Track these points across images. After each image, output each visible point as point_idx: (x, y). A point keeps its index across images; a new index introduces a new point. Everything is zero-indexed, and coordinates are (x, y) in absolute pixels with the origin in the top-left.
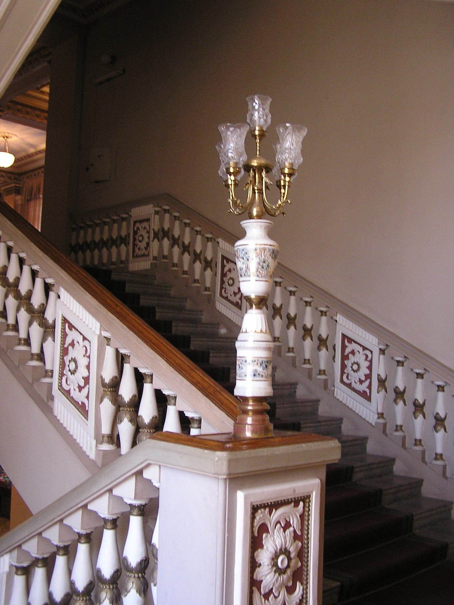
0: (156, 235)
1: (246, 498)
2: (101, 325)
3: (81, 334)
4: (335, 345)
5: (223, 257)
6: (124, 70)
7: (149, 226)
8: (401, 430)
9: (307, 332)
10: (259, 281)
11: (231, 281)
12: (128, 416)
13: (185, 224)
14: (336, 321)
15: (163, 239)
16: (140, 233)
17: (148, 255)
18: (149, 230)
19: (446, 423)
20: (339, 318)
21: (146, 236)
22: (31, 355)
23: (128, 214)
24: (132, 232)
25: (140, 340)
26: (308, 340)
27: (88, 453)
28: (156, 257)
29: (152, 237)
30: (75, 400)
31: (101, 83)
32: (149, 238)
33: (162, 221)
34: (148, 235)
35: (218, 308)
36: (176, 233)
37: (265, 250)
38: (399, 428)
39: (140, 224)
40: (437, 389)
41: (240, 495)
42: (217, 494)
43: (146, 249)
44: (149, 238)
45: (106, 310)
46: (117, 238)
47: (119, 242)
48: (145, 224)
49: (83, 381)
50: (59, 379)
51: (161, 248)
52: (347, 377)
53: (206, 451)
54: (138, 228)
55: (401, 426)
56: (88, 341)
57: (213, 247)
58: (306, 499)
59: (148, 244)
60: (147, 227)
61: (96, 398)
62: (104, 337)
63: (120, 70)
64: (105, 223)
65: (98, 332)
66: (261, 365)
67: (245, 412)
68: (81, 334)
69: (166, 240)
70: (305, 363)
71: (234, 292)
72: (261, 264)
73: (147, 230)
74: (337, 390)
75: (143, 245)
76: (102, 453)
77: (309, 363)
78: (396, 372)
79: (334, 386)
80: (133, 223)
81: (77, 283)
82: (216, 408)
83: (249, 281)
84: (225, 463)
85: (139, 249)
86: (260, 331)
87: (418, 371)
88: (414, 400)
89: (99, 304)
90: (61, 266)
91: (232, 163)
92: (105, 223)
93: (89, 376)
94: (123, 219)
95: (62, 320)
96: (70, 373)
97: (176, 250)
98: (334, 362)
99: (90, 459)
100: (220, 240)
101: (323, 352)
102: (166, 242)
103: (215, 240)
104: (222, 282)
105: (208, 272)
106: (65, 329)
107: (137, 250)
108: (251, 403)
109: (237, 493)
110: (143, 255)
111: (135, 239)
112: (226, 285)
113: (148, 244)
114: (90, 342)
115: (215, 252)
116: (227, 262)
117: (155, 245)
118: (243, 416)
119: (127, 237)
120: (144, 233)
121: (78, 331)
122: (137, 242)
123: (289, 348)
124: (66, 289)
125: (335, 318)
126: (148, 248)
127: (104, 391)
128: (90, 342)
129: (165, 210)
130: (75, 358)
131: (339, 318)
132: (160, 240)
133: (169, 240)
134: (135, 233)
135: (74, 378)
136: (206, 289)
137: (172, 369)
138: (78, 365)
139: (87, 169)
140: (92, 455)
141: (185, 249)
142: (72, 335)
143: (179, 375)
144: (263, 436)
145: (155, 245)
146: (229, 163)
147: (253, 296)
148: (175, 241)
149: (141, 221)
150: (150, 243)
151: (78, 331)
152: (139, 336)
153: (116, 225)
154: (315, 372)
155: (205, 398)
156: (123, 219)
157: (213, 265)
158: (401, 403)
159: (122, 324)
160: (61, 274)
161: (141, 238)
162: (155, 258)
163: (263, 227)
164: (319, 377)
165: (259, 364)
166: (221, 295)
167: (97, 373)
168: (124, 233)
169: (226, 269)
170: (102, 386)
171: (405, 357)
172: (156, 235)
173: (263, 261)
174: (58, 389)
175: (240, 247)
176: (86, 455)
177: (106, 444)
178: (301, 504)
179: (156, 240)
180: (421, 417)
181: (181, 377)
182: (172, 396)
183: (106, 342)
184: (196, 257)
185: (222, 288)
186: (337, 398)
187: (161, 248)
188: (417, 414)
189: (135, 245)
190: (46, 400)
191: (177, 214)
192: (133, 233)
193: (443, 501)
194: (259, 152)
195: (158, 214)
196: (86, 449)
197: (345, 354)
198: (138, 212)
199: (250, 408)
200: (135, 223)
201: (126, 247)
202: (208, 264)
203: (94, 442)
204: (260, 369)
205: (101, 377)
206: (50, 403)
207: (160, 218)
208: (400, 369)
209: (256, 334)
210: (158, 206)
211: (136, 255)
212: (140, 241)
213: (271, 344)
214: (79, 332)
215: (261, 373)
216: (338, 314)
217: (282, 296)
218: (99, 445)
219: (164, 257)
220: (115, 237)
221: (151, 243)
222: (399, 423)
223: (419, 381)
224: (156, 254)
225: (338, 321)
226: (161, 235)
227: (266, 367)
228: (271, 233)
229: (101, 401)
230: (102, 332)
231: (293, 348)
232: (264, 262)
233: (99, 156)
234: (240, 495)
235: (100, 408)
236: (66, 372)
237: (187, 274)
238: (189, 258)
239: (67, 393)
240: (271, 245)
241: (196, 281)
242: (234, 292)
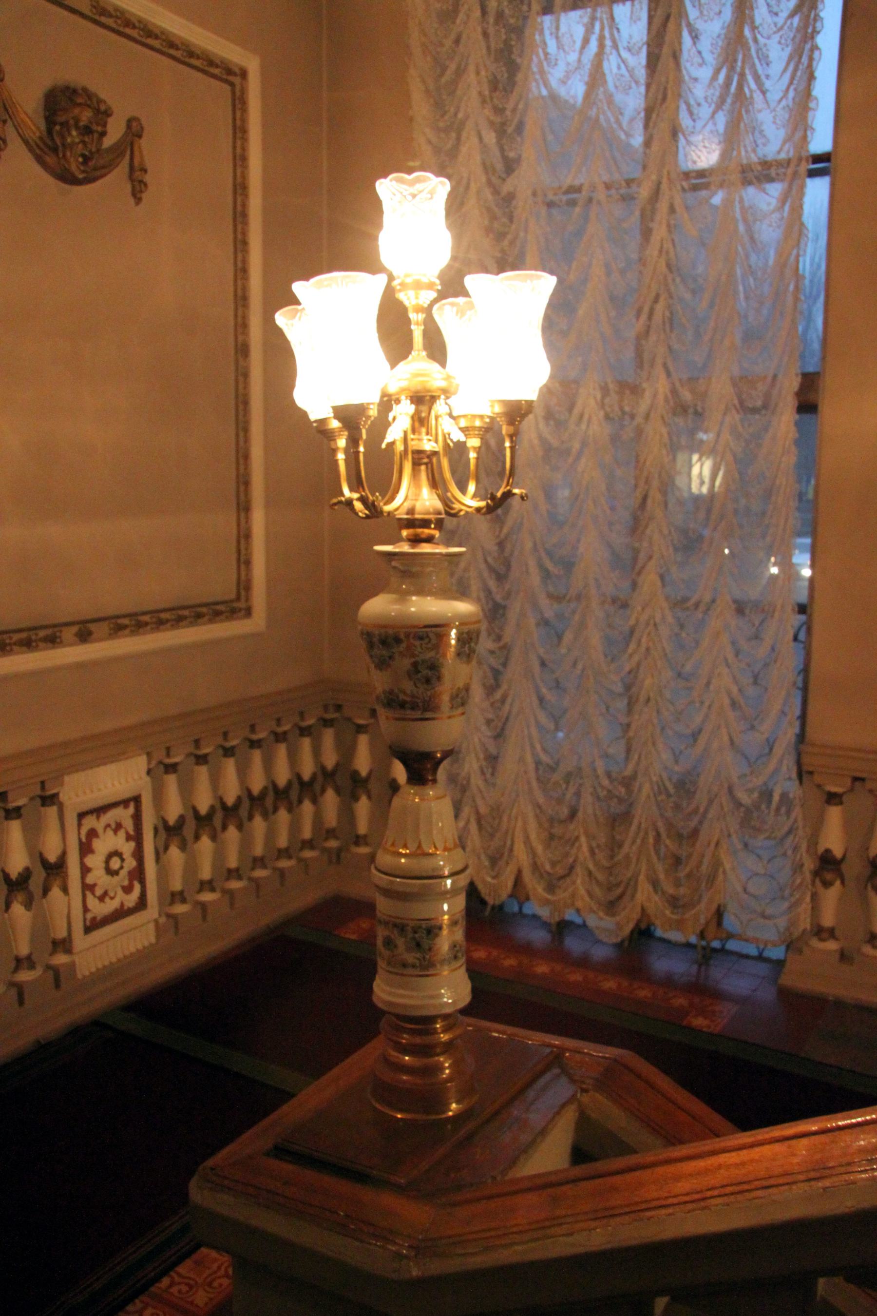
21: (98, 876)
32: (85, 870)
60: (92, 902)
73: (93, 894)
75: (104, 844)
107: (129, 825)
113: (86, 849)
122: (128, 848)
126: (84, 840)
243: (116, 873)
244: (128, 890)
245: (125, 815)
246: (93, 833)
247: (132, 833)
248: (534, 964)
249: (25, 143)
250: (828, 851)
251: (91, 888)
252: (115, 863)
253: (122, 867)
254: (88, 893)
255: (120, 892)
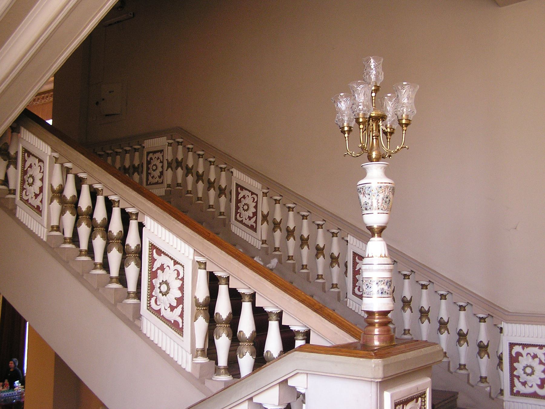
0: (170, 165)
1: (392, 396)
2: (194, 250)
3: (172, 259)
4: (347, 262)
5: (238, 186)
6: (133, 14)
7: (163, 156)
8: (409, 333)
9: (319, 251)
10: (383, 213)
11: (246, 207)
12: (225, 332)
13: (199, 155)
14: (347, 241)
15: (177, 169)
16: (153, 163)
17: (162, 183)
18: (163, 160)
19: (448, 325)
20: (350, 238)
22: (127, 293)
23: (140, 145)
24: (146, 162)
25: (241, 264)
26: (321, 258)
27: (184, 366)
28: (170, 185)
29: (166, 167)
30: (167, 318)
31: (110, 25)
32: (162, 167)
33: (175, 152)
34: (161, 164)
35: (233, 231)
36: (190, 163)
37: (387, 187)
38: (407, 332)
39: (153, 155)
40: (440, 297)
41: (387, 395)
42: (370, 395)
43: (160, 177)
44: (162, 167)
45: (201, 237)
46: (129, 167)
47: (131, 170)
48: (159, 155)
49: (175, 301)
50: (148, 300)
51: (175, 177)
52: (359, 290)
53: (361, 359)
54: (151, 159)
55: (409, 330)
56: (181, 265)
57: (226, 178)
58: (422, 395)
59: (162, 173)
61: (191, 317)
62: (197, 261)
63: (131, 14)
64: (117, 153)
65: (191, 257)
66: (386, 284)
67: (372, 324)
68: (172, 259)
69: (179, 169)
70: (318, 278)
71: (249, 216)
72: (385, 199)
74: (350, 301)
75: (157, 173)
76: (199, 366)
77: (322, 278)
78: (403, 284)
79: (346, 298)
80: (146, 153)
81: (165, 213)
82: (326, 321)
83: (373, 213)
84: (381, 369)
85: (153, 177)
86: (384, 256)
87: (423, 283)
88: (420, 307)
89: (193, 232)
90: (147, 198)
91: (361, 115)
92: (117, 153)
93: (183, 296)
94: (136, 150)
95: (149, 246)
96: (161, 294)
97: (190, 179)
98: (347, 277)
99: (187, 372)
100: (233, 170)
101: (336, 269)
102: (180, 171)
103: (228, 170)
104: (237, 208)
105: (223, 199)
106: (152, 254)
107: (150, 178)
108: (377, 314)
109: (383, 393)
110: (157, 183)
111: (148, 169)
112: (26, 186)
113: (162, 173)
114: (183, 266)
115: (229, 180)
116: (29, 156)
117: (169, 175)
118: (371, 328)
119: (140, 167)
120: (158, 163)
121: (168, 256)
122: (151, 171)
123: (303, 266)
124: (152, 218)
125: (346, 238)
126: (162, 176)
127: (197, 310)
128: (183, 266)
129: (178, 142)
130: (166, 281)
131: (350, 238)
132: (174, 170)
133: (182, 169)
134: (149, 163)
135: (166, 299)
136: (221, 214)
137: (279, 290)
138: (171, 287)
139: (97, 103)
140: (189, 369)
141: (199, 177)
142: (160, 260)
143: (286, 294)
144: (389, 345)
145: (169, 175)
146: (358, 114)
147: (375, 226)
148: (188, 171)
149: (154, 152)
150: (164, 172)
151: (168, 256)
152: (240, 261)
153: (128, 155)
154: (328, 286)
155: (315, 313)
156: (136, 150)
157: (227, 192)
158: (408, 310)
159: (219, 250)
160: (148, 204)
161: (154, 168)
162: (169, 186)
163: (383, 168)
164: (333, 290)
165: (385, 283)
166: (236, 219)
167: (192, 294)
168: (137, 163)
169: (27, 165)
170: (196, 306)
171: (412, 271)
172: (170, 165)
173: (386, 197)
174: (146, 309)
175: (361, 186)
176: (182, 368)
177: (200, 357)
178: (420, 399)
179: (170, 169)
180: (426, 321)
181: (288, 296)
182: (274, 313)
183: (198, 266)
184: (210, 185)
185: (237, 213)
186: (350, 307)
187: (175, 177)
188: (423, 319)
189: (148, 174)
190: (131, 319)
191: (190, 146)
192: (147, 163)
193: (449, 392)
194: (375, 103)
195: (171, 146)
196: (182, 362)
197: (356, 270)
198: (151, 144)
199: (376, 321)
200: (148, 153)
201: (139, 175)
202: (221, 192)
203: (190, 356)
204: (386, 288)
205: (195, 297)
206: (137, 322)
207: (173, 149)
208: (407, 281)
209: (382, 258)
210: (172, 139)
211: (150, 183)
212: (154, 170)
213: (391, 266)
214: (170, 257)
215: (387, 291)
216: (349, 235)
217: (295, 220)
218: (194, 359)
219: (178, 185)
220: (127, 166)
221: (165, 172)
222: (407, 327)
223: (424, 291)
224: (169, 182)
225: (349, 242)
226: (174, 165)
227: (390, 286)
228: (387, 173)
229: (196, 319)
230: (195, 257)
231: (306, 266)
232: (387, 198)
233: (110, 92)
234: (387, 395)
235: (194, 324)
236: (156, 293)
237: (201, 200)
238: (203, 186)
239: (158, 313)
240: (390, 183)
241: (210, 207)
242: (249, 216)
243: (154, 165)
244: (151, 159)
245: (518, 387)
246: (160, 177)
247: (149, 175)
248: (240, 344)
249: (124, 159)
250: (461, 330)
251: (161, 162)
252: (246, 207)
253: (159, 288)
254: (162, 161)
255: (153, 158)
